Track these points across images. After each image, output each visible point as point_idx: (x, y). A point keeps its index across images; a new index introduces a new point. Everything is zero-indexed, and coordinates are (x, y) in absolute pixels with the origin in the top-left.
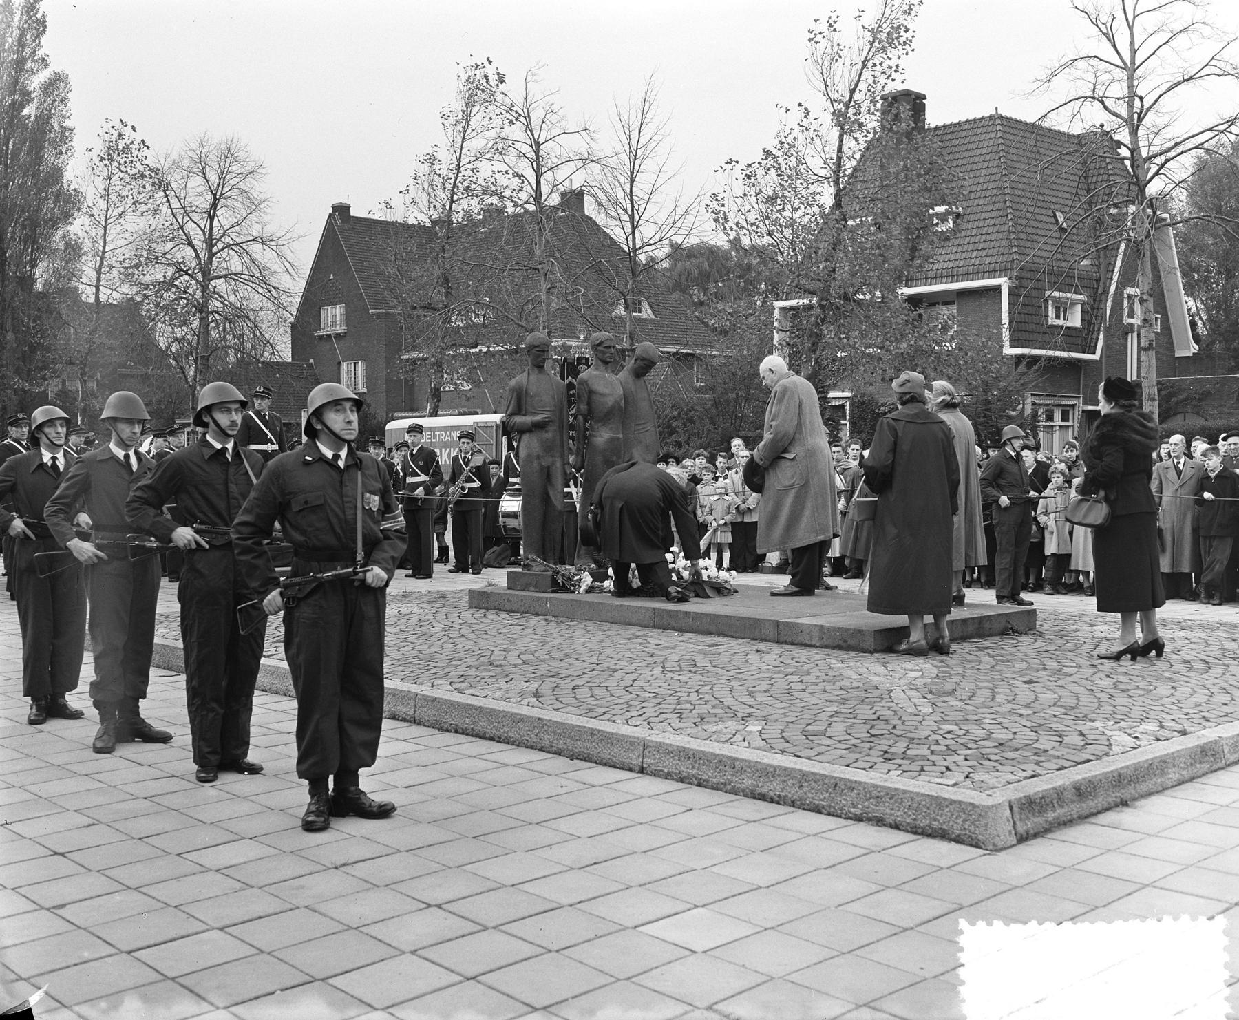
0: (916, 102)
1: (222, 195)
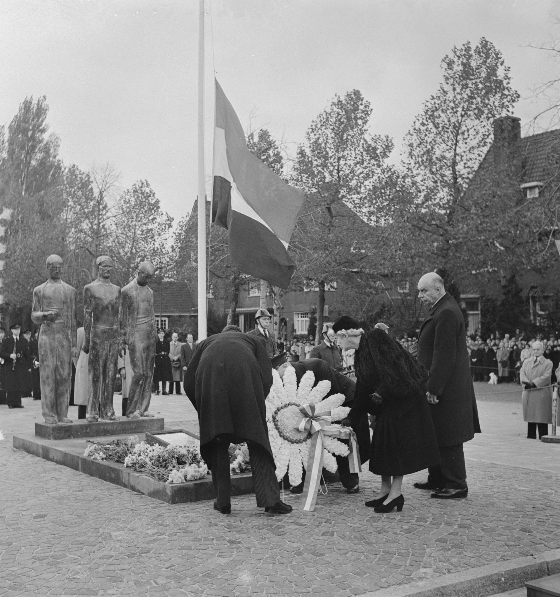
0: (515, 123)
1: (105, 190)
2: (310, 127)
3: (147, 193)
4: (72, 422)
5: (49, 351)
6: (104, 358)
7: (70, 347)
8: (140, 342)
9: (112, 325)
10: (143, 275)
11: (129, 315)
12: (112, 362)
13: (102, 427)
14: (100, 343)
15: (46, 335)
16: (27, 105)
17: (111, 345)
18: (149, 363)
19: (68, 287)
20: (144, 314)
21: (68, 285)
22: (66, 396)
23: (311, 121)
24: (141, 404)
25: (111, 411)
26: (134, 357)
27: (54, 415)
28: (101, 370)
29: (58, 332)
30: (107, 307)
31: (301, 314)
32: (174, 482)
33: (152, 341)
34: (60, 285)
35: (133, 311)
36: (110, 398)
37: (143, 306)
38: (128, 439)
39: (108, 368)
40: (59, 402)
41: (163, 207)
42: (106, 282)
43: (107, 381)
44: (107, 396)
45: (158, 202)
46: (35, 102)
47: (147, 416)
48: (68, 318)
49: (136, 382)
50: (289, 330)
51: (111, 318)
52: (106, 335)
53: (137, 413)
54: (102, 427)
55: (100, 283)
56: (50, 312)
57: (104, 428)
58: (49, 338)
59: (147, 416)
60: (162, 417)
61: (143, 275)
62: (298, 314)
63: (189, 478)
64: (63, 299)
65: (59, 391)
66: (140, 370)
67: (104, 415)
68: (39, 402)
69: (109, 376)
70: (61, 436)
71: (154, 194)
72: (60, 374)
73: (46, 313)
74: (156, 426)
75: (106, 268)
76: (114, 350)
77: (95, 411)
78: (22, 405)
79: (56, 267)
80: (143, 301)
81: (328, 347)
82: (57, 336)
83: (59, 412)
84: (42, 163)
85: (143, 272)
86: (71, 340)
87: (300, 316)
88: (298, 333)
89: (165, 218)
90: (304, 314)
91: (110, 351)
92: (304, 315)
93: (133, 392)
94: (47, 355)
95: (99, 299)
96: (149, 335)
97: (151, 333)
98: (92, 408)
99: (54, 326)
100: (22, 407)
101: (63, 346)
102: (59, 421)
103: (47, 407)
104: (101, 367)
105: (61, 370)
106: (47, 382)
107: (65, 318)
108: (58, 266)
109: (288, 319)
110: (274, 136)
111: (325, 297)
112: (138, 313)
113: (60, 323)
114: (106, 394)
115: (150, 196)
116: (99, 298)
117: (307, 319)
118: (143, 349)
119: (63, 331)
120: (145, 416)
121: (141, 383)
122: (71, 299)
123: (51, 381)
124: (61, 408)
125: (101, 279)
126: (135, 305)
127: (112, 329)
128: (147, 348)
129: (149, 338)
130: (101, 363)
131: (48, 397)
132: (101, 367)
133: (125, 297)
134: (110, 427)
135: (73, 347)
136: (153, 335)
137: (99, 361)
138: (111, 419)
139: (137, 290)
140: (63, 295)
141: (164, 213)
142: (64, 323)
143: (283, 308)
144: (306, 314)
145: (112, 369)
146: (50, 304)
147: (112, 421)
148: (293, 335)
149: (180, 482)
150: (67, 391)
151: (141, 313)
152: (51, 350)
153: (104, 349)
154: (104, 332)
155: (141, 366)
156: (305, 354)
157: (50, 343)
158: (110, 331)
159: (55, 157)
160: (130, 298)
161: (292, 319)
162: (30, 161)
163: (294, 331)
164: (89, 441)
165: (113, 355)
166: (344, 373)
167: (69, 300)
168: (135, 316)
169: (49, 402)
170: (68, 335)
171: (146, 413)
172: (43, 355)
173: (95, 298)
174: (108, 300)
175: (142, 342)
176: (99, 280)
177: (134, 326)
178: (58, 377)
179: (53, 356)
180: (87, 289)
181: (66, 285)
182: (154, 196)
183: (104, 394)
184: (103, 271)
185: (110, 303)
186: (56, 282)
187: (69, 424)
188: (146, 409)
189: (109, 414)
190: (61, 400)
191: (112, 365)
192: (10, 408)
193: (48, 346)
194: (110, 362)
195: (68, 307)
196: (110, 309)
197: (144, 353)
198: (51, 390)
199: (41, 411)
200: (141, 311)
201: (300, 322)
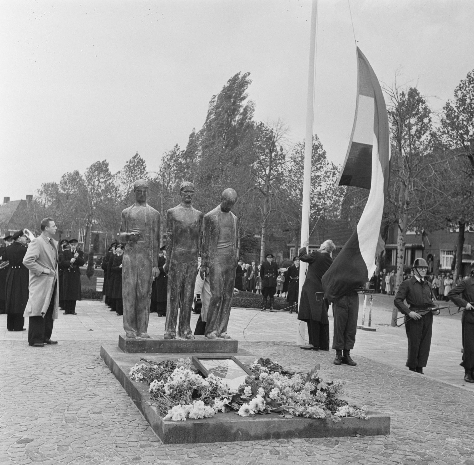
2: (458, 85)
3: (317, 145)
4: (149, 337)
5: (130, 270)
6: (181, 279)
7: (151, 266)
8: (219, 265)
9: (191, 247)
10: (225, 201)
11: (211, 239)
12: (189, 283)
13: (175, 345)
14: (178, 264)
15: (129, 254)
16: (234, 80)
17: (188, 267)
18: (227, 287)
19: (152, 210)
20: (225, 239)
21: (152, 208)
22: (144, 313)
23: (460, 80)
24: (219, 325)
25: (188, 330)
26: (213, 280)
27: (133, 330)
28: (179, 290)
29: (140, 252)
30: (185, 231)
31: (447, 251)
32: (174, 419)
33: (232, 266)
34: (145, 208)
35: (215, 236)
36: (187, 317)
37: (224, 231)
38: (177, 360)
39: (186, 289)
40: (138, 318)
41: (329, 158)
42: (188, 207)
43: (185, 301)
44: (185, 315)
45: (324, 153)
46: (240, 77)
47: (223, 337)
48: (150, 239)
49: (213, 303)
50: (435, 265)
51: (189, 241)
52: (183, 257)
53: (213, 333)
54: (175, 345)
55: (182, 207)
56: (132, 233)
57: (177, 346)
58: (130, 257)
59: (223, 337)
60: (236, 339)
61: (225, 201)
62: (444, 251)
63: (191, 416)
64: (146, 221)
65: (139, 308)
66: (217, 292)
67: (181, 333)
68: (121, 317)
69: (186, 297)
70: (134, 350)
71: (322, 146)
72: (140, 292)
73: (129, 234)
74: (229, 348)
75: (187, 193)
76: (192, 271)
77: (171, 328)
78: (76, 312)
79: (141, 191)
80: (225, 226)
81: (417, 281)
82: (139, 256)
83: (138, 326)
84: (241, 123)
85: (225, 199)
86: (152, 261)
87: (445, 253)
88: (444, 267)
89: (330, 166)
90: (449, 251)
91: (187, 273)
92: (449, 252)
93: (210, 313)
94: (128, 273)
95: (180, 222)
96: (228, 259)
97: (231, 258)
98: (169, 325)
99: (136, 246)
100: (76, 314)
101: (143, 266)
102: (138, 335)
103: (128, 321)
104: (178, 287)
105: (140, 287)
106: (128, 298)
107: (147, 240)
108: (143, 190)
109: (434, 255)
110: (422, 93)
111: (465, 237)
112: (218, 238)
113: (142, 243)
114: (183, 313)
115: (318, 148)
116: (179, 222)
117: (452, 256)
118: (222, 273)
119: (144, 251)
120: (221, 337)
121: (217, 305)
122: (153, 222)
123: (131, 297)
124: (140, 324)
125: (183, 204)
126: (216, 230)
127: (189, 252)
128: (226, 272)
129: (228, 262)
130: (178, 283)
131: (128, 312)
132: (178, 287)
133: (209, 221)
134: (183, 345)
135: (154, 267)
136: (233, 260)
137: (176, 282)
138: (187, 338)
139: (219, 216)
140: (146, 217)
141: (330, 163)
142: (145, 243)
143: (430, 246)
144: (451, 251)
145: (190, 290)
146: (133, 226)
147: (186, 340)
148: (438, 269)
149: (180, 419)
150: (145, 308)
151: (222, 238)
152: (132, 268)
153: (181, 271)
154: (182, 254)
155: (218, 289)
156: (444, 286)
157: (132, 262)
158: (187, 253)
159: (250, 119)
160: (212, 223)
161: (438, 256)
162: (231, 122)
163: (439, 265)
164: (143, 359)
165: (190, 277)
166: (433, 309)
167: (151, 223)
168: (216, 241)
169: (129, 318)
170: (149, 255)
171: (223, 334)
172: (125, 273)
173: (176, 221)
174: (187, 224)
175: (221, 266)
176: (182, 205)
177: (215, 250)
178: (138, 294)
179: (134, 275)
180: (170, 213)
181: (151, 208)
182: (322, 148)
183: (182, 313)
184: (185, 196)
185: (189, 227)
186: (141, 205)
187: (145, 339)
188: (224, 330)
189: (186, 333)
190: (141, 315)
191: (189, 286)
192: (159, 316)
193: (129, 264)
194: (187, 283)
195: (150, 229)
196: (189, 233)
197: (223, 276)
198: (131, 306)
199: (122, 325)
200: (222, 235)
201: (445, 258)
